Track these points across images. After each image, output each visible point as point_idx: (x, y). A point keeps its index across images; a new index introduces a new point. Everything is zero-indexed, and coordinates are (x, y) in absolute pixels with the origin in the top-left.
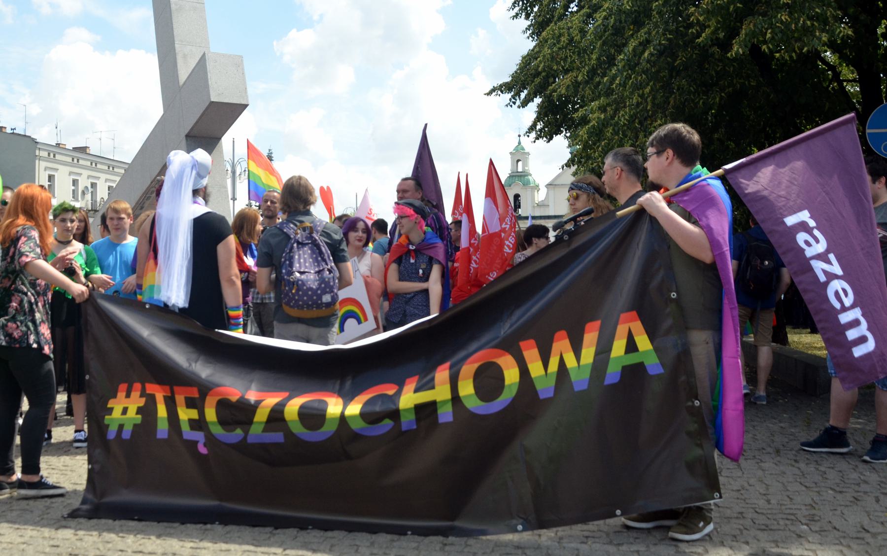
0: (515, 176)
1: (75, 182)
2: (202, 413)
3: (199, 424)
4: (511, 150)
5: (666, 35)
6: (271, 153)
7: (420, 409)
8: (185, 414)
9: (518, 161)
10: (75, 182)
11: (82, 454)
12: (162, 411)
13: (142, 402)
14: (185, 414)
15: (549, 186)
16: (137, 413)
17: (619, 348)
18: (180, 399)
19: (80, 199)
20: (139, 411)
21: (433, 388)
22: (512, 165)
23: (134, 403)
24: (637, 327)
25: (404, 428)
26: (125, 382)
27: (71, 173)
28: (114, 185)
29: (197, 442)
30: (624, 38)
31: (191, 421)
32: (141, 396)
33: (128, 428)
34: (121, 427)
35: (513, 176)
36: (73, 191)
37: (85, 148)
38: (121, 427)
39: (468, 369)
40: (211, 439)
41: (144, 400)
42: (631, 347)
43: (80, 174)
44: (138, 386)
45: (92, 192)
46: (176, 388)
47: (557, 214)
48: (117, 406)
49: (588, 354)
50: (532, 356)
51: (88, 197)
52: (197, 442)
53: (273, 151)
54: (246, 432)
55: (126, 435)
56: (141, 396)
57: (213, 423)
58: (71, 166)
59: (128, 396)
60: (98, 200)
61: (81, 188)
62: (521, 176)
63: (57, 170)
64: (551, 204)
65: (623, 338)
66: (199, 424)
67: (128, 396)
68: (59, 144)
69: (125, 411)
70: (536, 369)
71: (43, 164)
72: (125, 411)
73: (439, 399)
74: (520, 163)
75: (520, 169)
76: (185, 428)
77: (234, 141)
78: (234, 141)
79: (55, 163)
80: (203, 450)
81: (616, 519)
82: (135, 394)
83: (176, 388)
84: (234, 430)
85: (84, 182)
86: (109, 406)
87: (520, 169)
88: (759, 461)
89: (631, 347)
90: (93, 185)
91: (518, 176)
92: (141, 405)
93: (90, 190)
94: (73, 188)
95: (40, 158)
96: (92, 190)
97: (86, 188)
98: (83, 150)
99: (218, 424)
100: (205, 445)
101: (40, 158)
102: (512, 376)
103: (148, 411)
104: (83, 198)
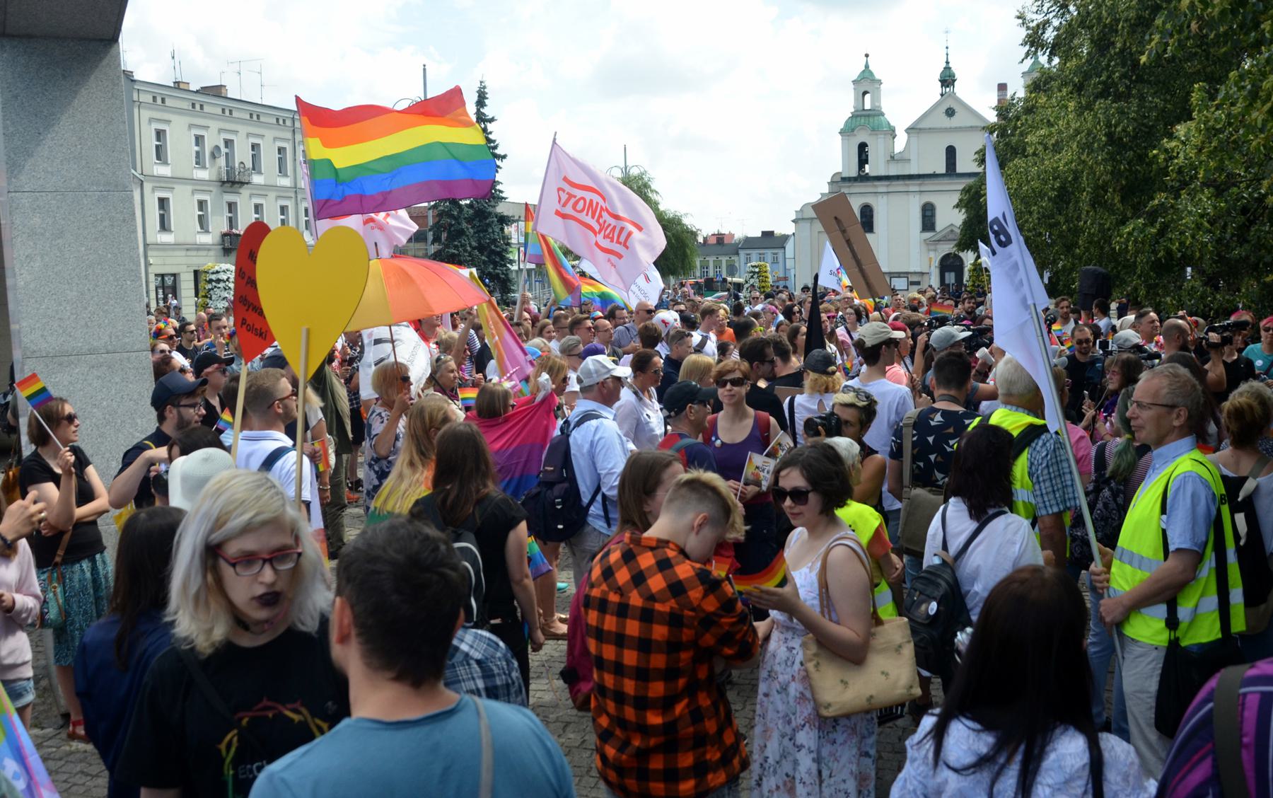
0: (861, 116)
1: (199, 140)
4: (855, 77)
6: (484, 87)
9: (865, 93)
10: (199, 140)
11: (598, 622)
15: (910, 130)
19: (207, 165)
22: (856, 99)
27: (191, 126)
35: (857, 116)
36: (197, 153)
43: (236, 132)
45: (227, 154)
47: (921, 173)
51: (222, 161)
53: (486, 84)
58: (222, 120)
62: (869, 116)
63: (168, 122)
64: (913, 157)
68: (178, 83)
71: (146, 114)
74: (868, 97)
75: (868, 106)
77: (424, 70)
78: (424, 70)
79: (205, 117)
85: (213, 139)
87: (868, 106)
90: (228, 143)
91: (865, 116)
93: (224, 150)
94: (197, 148)
96: (227, 150)
97: (217, 148)
98: (216, 91)
104: (213, 164)
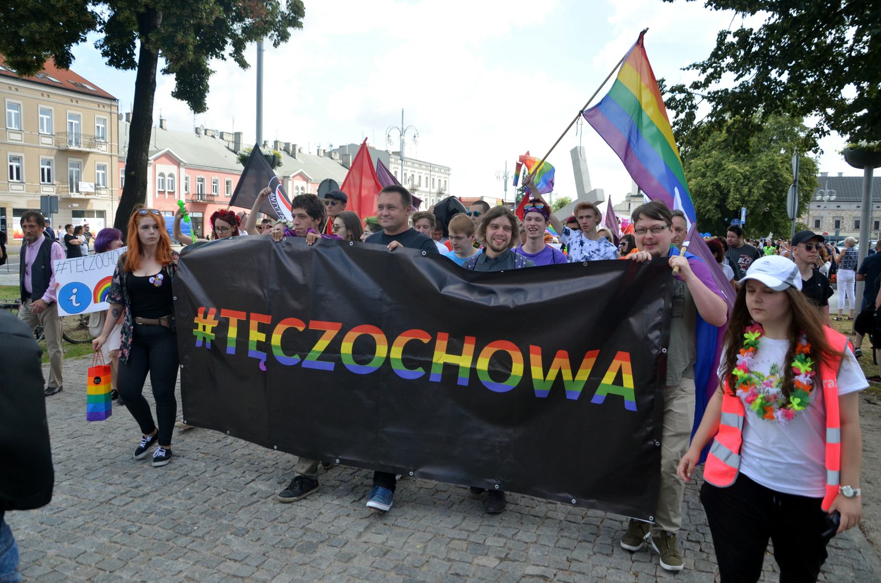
2: (269, 338)
3: (264, 346)
5: (328, 205)
8: (256, 336)
12: (232, 333)
13: (215, 324)
14: (256, 336)
17: (609, 378)
18: (253, 324)
20: (214, 330)
21: (460, 354)
23: (210, 324)
24: (627, 366)
25: (431, 379)
29: (260, 360)
30: (329, 537)
31: (259, 343)
39: (488, 351)
40: (271, 359)
41: (217, 322)
42: (618, 381)
46: (252, 315)
49: (584, 375)
50: (536, 360)
52: (260, 360)
54: (303, 358)
57: (276, 347)
61: (408, 178)
65: (615, 372)
66: (264, 346)
70: (537, 372)
73: (461, 365)
76: (252, 347)
80: (263, 368)
82: (211, 317)
83: (252, 315)
84: (294, 355)
89: (618, 381)
90: (413, 175)
92: (215, 326)
95: (392, 163)
100: (265, 364)
101: (392, 163)
102: (518, 369)
103: (221, 328)
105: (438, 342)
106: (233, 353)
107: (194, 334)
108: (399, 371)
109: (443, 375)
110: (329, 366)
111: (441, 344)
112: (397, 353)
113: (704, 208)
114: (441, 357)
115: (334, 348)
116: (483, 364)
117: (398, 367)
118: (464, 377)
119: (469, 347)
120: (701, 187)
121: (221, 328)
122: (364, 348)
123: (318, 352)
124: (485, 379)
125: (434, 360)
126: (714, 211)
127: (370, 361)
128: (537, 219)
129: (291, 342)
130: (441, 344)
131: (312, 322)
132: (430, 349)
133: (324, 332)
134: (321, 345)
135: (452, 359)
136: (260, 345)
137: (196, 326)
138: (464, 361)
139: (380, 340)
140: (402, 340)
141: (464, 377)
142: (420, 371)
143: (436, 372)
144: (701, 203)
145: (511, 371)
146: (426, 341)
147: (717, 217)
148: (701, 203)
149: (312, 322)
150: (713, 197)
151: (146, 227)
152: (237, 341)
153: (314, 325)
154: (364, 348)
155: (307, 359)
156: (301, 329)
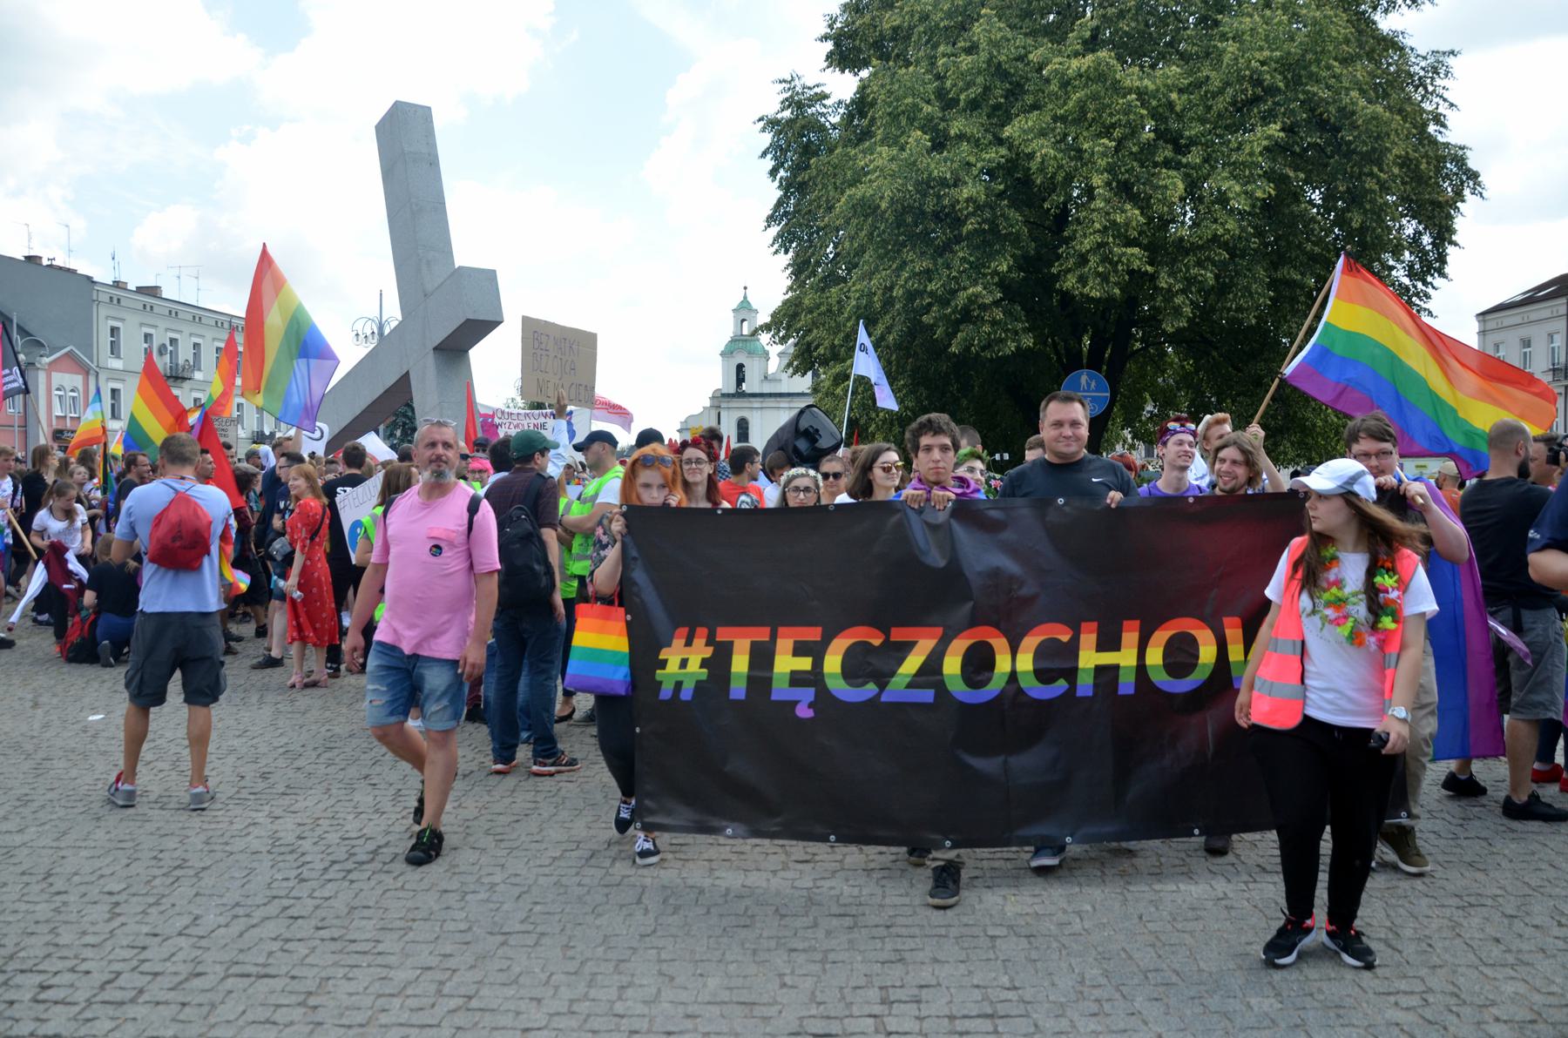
1: (148, 337)
3: (814, 678)
7: (1100, 670)
9: (743, 320)
10: (148, 337)
12: (740, 664)
13: (708, 652)
14: (786, 663)
16: (702, 666)
22: (735, 326)
25: (1079, 693)
26: (684, 626)
28: (222, 345)
32: (707, 645)
33: (689, 686)
34: (679, 684)
37: (157, 288)
38: (679, 684)
39: (1161, 637)
40: (824, 697)
44: (702, 631)
48: (672, 657)
50: (1234, 634)
54: (882, 686)
55: (687, 694)
56: (707, 645)
57: (832, 675)
59: (689, 643)
60: (181, 362)
66: (814, 678)
67: (689, 643)
69: (684, 663)
72: (684, 663)
73: (1122, 664)
74: (745, 324)
81: (1193, 839)
82: (699, 642)
84: (866, 683)
86: (661, 657)
88: (62, 909)
90: (173, 341)
92: (708, 655)
94: (146, 345)
98: (153, 291)
99: (1033, 676)
103: (719, 662)
105: (1083, 637)
106: (743, 697)
107: (658, 678)
108: (1031, 689)
109: (1095, 685)
110: (927, 695)
111: (1088, 639)
112: (1025, 663)
113: (945, 303)
114: (1089, 658)
115: (932, 668)
116: (1155, 656)
117: (1029, 683)
118: (1127, 682)
119: (1130, 638)
120: (926, 185)
121: (719, 662)
122: (979, 663)
123: (906, 676)
124: (1159, 677)
125: (1081, 664)
126: (999, 315)
127: (989, 680)
128: (1190, 445)
129: (858, 666)
130: (1088, 639)
131: (894, 631)
132: (1072, 649)
133: (915, 643)
134: (912, 664)
135: (1108, 658)
136: (797, 679)
137: (663, 664)
138: (1125, 658)
139: (1000, 644)
140: (1030, 643)
141: (1127, 682)
142: (1062, 684)
143: (1085, 682)
144: (928, 274)
145: (1197, 657)
146: (1065, 638)
147: (1013, 346)
148: (928, 274)
149: (894, 631)
150: (989, 239)
151: (647, 486)
152: (750, 679)
153: (898, 635)
154: (979, 663)
155: (889, 687)
156: (877, 642)
